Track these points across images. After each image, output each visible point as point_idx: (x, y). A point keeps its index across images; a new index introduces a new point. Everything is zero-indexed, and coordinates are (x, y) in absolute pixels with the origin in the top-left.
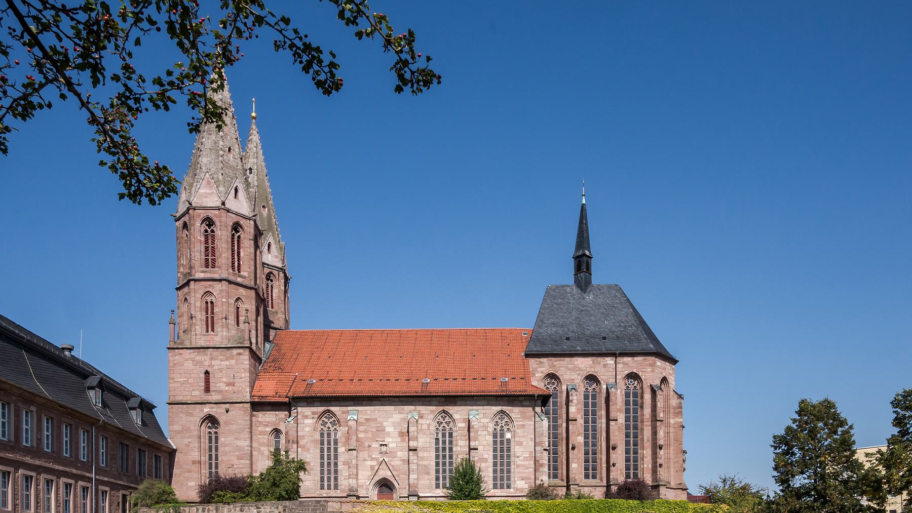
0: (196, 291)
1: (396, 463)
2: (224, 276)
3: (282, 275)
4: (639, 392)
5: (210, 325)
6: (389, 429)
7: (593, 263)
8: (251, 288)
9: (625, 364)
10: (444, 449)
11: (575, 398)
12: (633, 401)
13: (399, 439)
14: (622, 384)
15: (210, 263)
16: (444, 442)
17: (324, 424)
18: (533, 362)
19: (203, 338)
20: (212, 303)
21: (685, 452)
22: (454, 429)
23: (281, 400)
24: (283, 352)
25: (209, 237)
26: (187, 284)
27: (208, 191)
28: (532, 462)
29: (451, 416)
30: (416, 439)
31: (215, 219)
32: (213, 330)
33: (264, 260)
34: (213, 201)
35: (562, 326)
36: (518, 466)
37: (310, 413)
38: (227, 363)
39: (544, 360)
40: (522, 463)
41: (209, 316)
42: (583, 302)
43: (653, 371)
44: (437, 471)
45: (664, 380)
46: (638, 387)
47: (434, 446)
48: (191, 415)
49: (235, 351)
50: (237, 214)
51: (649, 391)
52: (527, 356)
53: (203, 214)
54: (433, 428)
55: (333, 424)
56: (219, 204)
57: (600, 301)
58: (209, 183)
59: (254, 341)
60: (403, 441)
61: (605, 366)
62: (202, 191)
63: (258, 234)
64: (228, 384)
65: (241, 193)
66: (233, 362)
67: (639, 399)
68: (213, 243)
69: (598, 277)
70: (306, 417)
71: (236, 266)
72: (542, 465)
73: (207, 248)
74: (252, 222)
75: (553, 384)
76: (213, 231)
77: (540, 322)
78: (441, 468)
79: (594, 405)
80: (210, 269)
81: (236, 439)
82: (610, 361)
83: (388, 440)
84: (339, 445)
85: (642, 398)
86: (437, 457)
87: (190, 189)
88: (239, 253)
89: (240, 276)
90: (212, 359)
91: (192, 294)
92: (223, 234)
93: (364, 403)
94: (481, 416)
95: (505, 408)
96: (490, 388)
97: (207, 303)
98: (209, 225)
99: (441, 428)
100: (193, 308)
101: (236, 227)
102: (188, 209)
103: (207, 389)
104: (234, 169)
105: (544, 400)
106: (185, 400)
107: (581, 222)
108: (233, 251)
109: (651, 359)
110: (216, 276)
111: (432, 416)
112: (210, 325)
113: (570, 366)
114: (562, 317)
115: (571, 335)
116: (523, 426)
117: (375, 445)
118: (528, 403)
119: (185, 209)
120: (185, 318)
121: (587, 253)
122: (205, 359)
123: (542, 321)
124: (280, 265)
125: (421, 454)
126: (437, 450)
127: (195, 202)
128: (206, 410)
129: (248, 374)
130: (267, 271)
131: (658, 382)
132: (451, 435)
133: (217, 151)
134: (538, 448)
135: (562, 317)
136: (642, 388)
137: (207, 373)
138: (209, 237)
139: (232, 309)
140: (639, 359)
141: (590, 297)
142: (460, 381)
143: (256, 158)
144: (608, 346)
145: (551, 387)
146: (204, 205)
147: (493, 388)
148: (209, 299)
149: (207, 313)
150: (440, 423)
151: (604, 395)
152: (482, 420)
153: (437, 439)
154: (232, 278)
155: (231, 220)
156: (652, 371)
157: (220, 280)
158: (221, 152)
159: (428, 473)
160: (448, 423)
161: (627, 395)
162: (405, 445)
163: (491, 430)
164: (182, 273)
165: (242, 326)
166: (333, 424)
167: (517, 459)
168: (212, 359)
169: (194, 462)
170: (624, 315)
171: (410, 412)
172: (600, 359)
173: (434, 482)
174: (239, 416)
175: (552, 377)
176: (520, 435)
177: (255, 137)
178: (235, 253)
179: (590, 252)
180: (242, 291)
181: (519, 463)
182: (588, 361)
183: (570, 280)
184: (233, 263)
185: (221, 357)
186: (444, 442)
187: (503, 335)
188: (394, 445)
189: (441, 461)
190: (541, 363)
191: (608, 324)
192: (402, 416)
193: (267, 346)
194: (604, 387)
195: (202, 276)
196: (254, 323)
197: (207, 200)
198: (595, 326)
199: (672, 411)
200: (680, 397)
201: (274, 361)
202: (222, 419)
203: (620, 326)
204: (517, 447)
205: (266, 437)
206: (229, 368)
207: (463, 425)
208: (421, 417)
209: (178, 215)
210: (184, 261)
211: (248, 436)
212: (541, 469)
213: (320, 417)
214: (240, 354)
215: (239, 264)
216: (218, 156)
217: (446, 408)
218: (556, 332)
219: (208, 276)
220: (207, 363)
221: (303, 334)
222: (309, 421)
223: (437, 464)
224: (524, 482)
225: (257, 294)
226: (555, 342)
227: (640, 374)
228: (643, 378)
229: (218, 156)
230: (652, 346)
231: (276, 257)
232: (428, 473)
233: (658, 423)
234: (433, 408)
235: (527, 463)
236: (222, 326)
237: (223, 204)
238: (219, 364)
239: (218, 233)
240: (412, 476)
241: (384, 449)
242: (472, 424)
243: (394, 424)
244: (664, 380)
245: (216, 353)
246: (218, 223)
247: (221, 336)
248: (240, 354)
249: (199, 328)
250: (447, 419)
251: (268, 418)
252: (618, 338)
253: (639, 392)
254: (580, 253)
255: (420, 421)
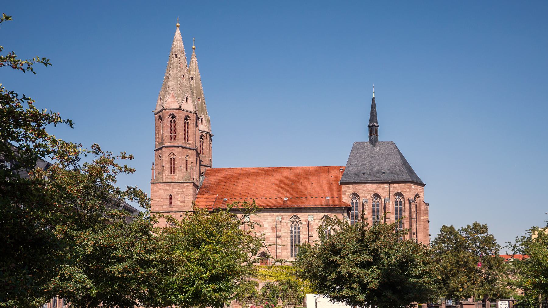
0: (166, 153)
2: (180, 145)
3: (208, 135)
4: (403, 203)
5: (173, 170)
6: (266, 225)
7: (379, 130)
8: (194, 150)
10: (295, 236)
11: (367, 207)
12: (399, 207)
14: (393, 199)
15: (173, 137)
16: (295, 232)
18: (344, 187)
19: (169, 177)
21: (430, 235)
24: (210, 181)
25: (173, 124)
26: (161, 148)
27: (173, 100)
29: (299, 218)
30: (280, 231)
31: (176, 115)
32: (174, 173)
33: (200, 129)
34: (175, 106)
35: (361, 166)
38: (181, 190)
39: (350, 186)
41: (172, 165)
42: (373, 152)
43: (410, 191)
44: (292, 248)
45: (417, 195)
47: (290, 234)
49: (185, 184)
50: (187, 111)
51: (408, 202)
52: (341, 183)
53: (170, 112)
54: (289, 225)
56: (178, 107)
57: (382, 151)
58: (173, 96)
59: (195, 177)
60: (273, 232)
61: (383, 189)
62: (169, 100)
63: (198, 118)
64: (181, 202)
65: (189, 100)
66: (184, 190)
68: (175, 127)
69: (382, 138)
71: (186, 139)
73: (171, 130)
74: (195, 115)
75: (356, 198)
76: (175, 121)
77: (349, 163)
78: (294, 238)
79: (378, 210)
82: (386, 186)
83: (265, 231)
85: (404, 206)
86: (292, 240)
87: (163, 99)
88: (188, 131)
90: (173, 188)
91: (164, 154)
92: (180, 123)
94: (315, 218)
95: (327, 214)
96: (320, 203)
98: (173, 118)
99: (293, 225)
100: (164, 162)
101: (187, 118)
102: (162, 110)
103: (171, 204)
104: (186, 86)
105: (349, 210)
107: (372, 107)
108: (185, 130)
109: (408, 185)
110: (176, 145)
111: (289, 219)
112: (173, 170)
113: (365, 189)
114: (361, 161)
115: (365, 171)
118: (339, 211)
119: (160, 109)
120: (159, 166)
121: (376, 124)
122: (169, 188)
123: (350, 163)
124: (207, 130)
125: (283, 239)
126: (292, 236)
127: (166, 106)
129: (192, 197)
130: (201, 134)
131: (413, 197)
132: (299, 228)
133: (177, 78)
135: (361, 161)
136: (404, 201)
137: (171, 196)
138: (173, 124)
139: (185, 162)
140: (403, 185)
141: (377, 149)
142: (304, 199)
143: (195, 73)
144: (386, 177)
145: (355, 201)
146: (171, 107)
147: (321, 203)
148: (172, 157)
150: (293, 222)
151: (383, 205)
152: (316, 221)
153: (292, 231)
154: (184, 145)
155: (183, 115)
156: (409, 191)
157: (178, 147)
158: (179, 79)
159: (287, 249)
160: (297, 222)
161: (396, 205)
162: (274, 234)
164: (158, 142)
165: (189, 170)
168: (173, 188)
170: (396, 160)
171: (277, 216)
172: (381, 185)
173: (290, 254)
175: (355, 195)
177: (195, 60)
178: (186, 132)
179: (377, 123)
180: (189, 151)
182: (375, 186)
183: (367, 140)
184: (185, 137)
186: (295, 232)
187: (329, 169)
188: (269, 234)
191: (386, 165)
192: (273, 218)
193: (201, 178)
194: (383, 200)
195: (168, 144)
196: (195, 168)
197: (172, 105)
198: (379, 166)
199: (422, 212)
200: (427, 204)
201: (205, 187)
203: (392, 166)
206: (182, 193)
207: (305, 223)
208: (283, 219)
209: (156, 112)
210: (159, 136)
214: (188, 186)
215: (188, 137)
216: (178, 81)
217: (296, 214)
218: (358, 170)
219: (172, 144)
221: (220, 170)
223: (292, 244)
225: (197, 152)
226: (357, 175)
227: (403, 193)
228: (404, 195)
229: (178, 81)
230: (409, 177)
231: (205, 126)
232: (287, 249)
233: (413, 220)
234: (290, 214)
236: (179, 171)
237: (180, 107)
238: (177, 191)
239: (177, 122)
240: (278, 251)
242: (310, 223)
243: (269, 223)
244: (417, 195)
245: (176, 185)
246: (177, 117)
247: (179, 176)
248: (188, 186)
249: (167, 172)
250: (297, 220)
252: (391, 172)
253: (403, 203)
254: (372, 125)
255: (283, 221)
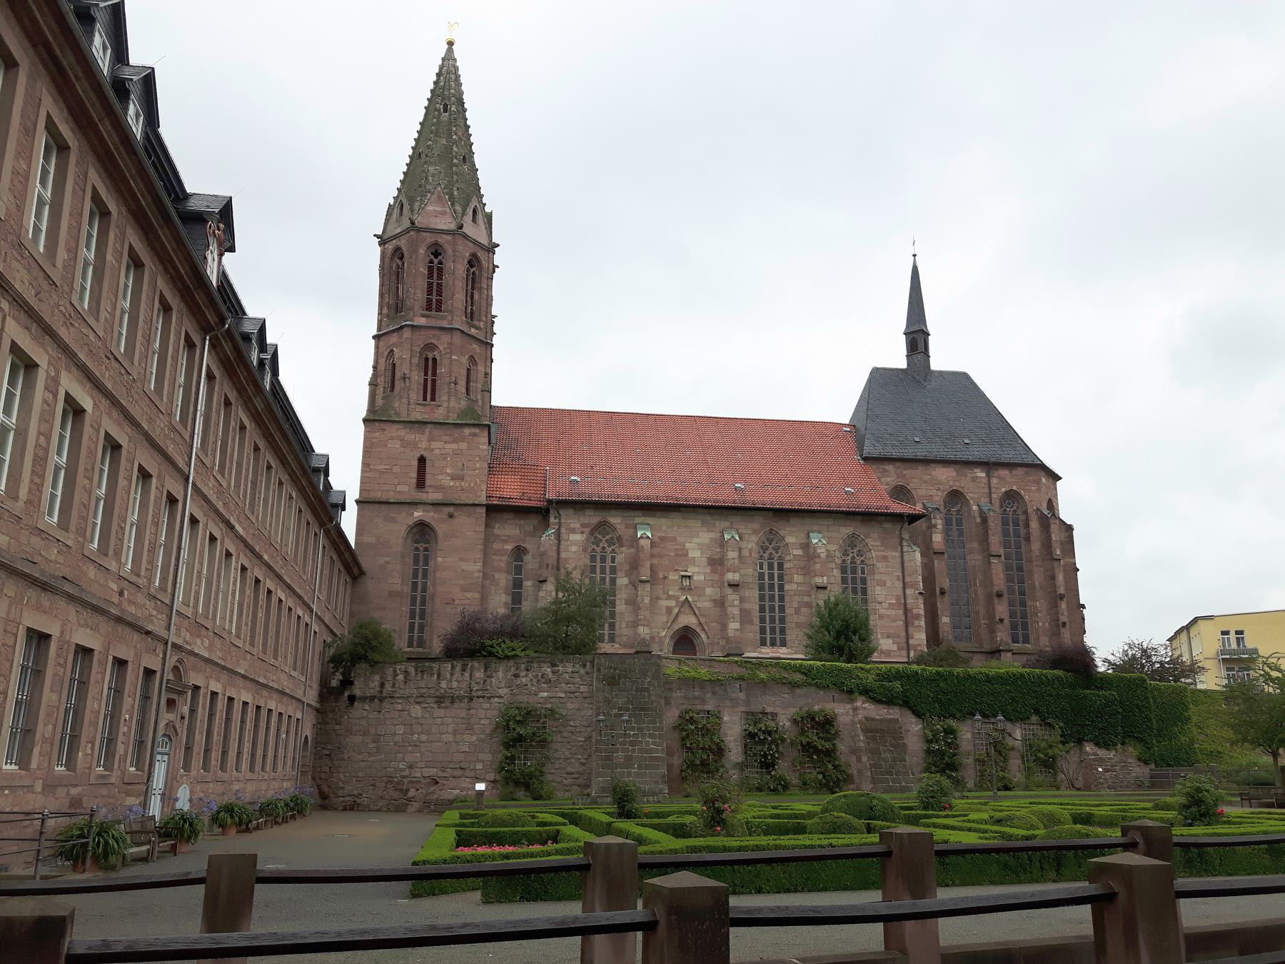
1: (705, 604)
6: (694, 554)
9: (1001, 479)
10: (771, 587)
13: (708, 570)
17: (597, 542)
19: (419, 408)
20: (434, 360)
22: (788, 558)
23: (532, 504)
28: (901, 612)
31: (446, 246)
32: (433, 399)
34: (446, 223)
36: (881, 617)
37: (578, 525)
38: (455, 446)
39: (890, 467)
40: (888, 612)
41: (429, 377)
44: (762, 620)
46: (1020, 512)
48: (393, 520)
49: (467, 431)
55: (610, 542)
64: (453, 478)
66: (464, 446)
67: (1021, 528)
70: (573, 531)
72: (918, 617)
73: (430, 285)
76: (440, 263)
80: (433, 313)
81: (462, 560)
84: (619, 574)
85: (1027, 526)
89: (474, 327)
93: (658, 514)
97: (427, 359)
98: (436, 254)
99: (766, 555)
103: (421, 483)
106: (384, 497)
110: (445, 324)
112: (430, 391)
113: (926, 477)
116: (885, 558)
117: (673, 577)
122: (421, 442)
128: (416, 514)
132: (781, 566)
134: (909, 592)
137: (422, 460)
146: (432, 226)
149: (426, 374)
150: (765, 549)
163: (838, 561)
166: (610, 542)
167: (878, 606)
168: (431, 439)
169: (391, 594)
174: (470, 527)
176: (883, 570)
181: (882, 611)
185: (447, 438)
186: (771, 577)
189: (767, 604)
190: (885, 471)
192: (712, 535)
195: (422, 321)
197: (437, 220)
202: (441, 528)
204: (878, 588)
205: (504, 558)
206: (456, 453)
211: (479, 555)
212: (916, 623)
213: (592, 533)
219: (433, 323)
220: (424, 445)
222: (577, 537)
223: (762, 609)
224: (890, 641)
234: (757, 526)
235: (893, 612)
239: (449, 265)
241: (686, 582)
243: (701, 547)
245: (438, 432)
246: (450, 252)
248: (474, 435)
249: (415, 395)
251: (509, 530)
